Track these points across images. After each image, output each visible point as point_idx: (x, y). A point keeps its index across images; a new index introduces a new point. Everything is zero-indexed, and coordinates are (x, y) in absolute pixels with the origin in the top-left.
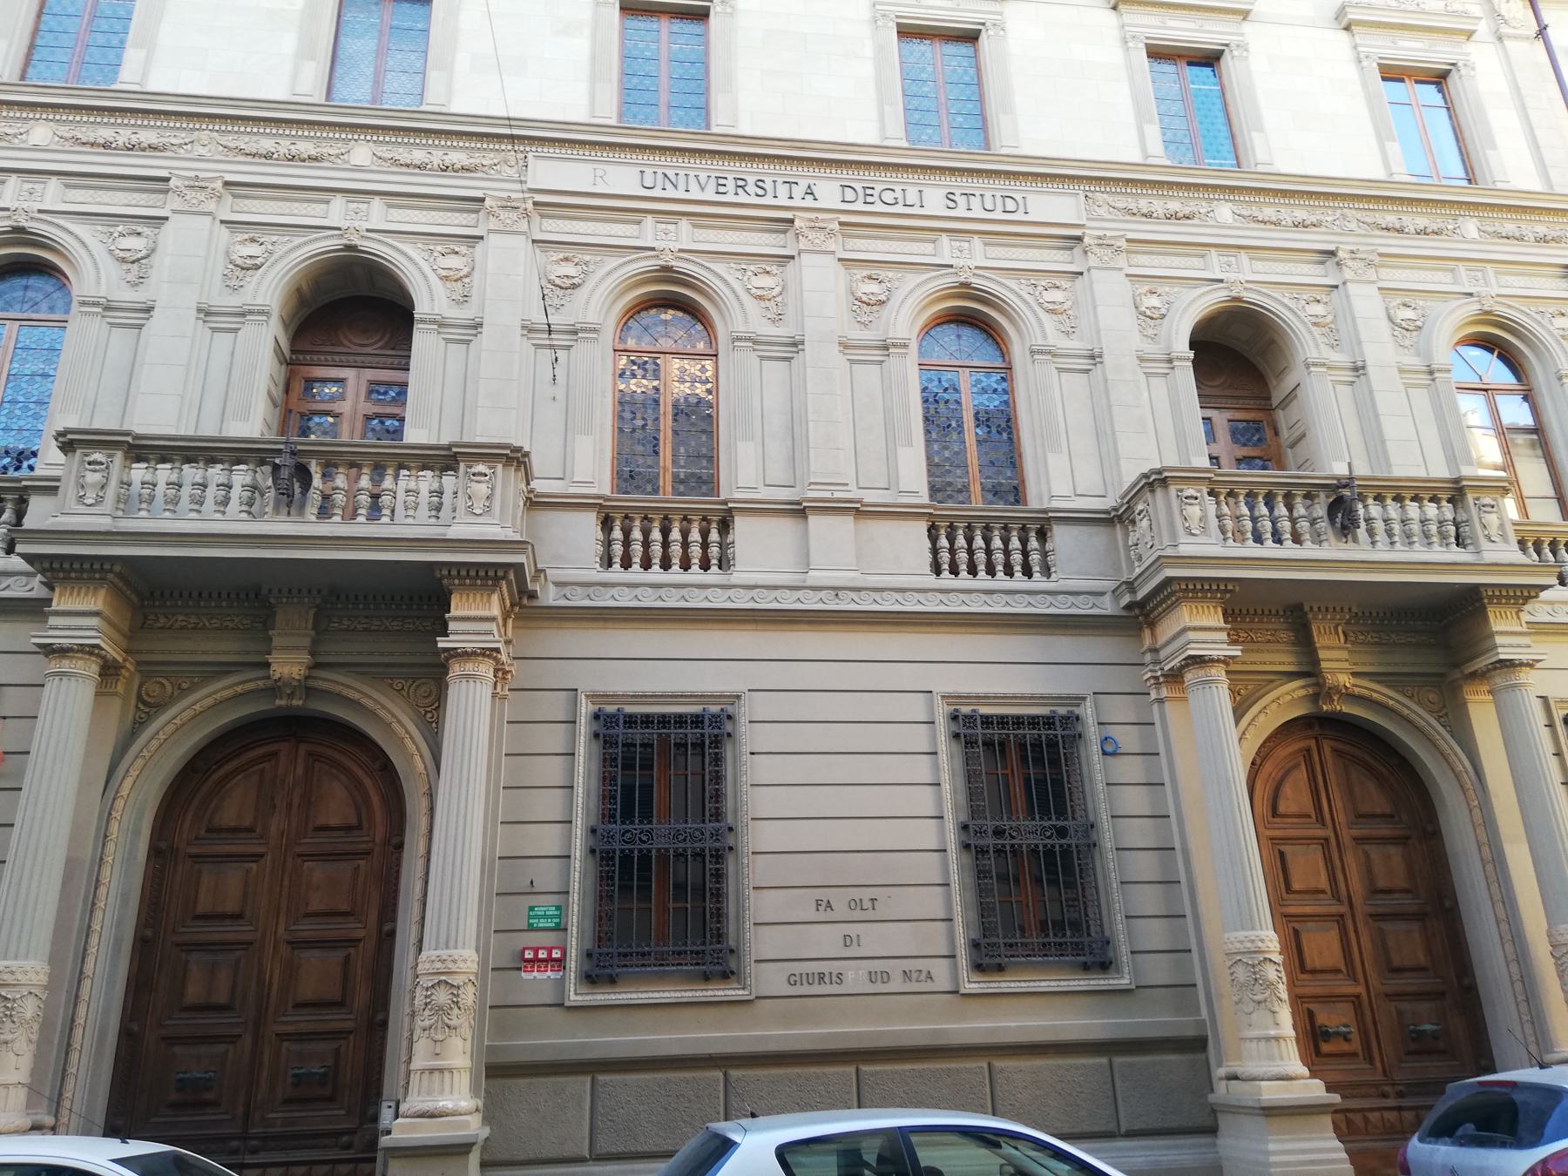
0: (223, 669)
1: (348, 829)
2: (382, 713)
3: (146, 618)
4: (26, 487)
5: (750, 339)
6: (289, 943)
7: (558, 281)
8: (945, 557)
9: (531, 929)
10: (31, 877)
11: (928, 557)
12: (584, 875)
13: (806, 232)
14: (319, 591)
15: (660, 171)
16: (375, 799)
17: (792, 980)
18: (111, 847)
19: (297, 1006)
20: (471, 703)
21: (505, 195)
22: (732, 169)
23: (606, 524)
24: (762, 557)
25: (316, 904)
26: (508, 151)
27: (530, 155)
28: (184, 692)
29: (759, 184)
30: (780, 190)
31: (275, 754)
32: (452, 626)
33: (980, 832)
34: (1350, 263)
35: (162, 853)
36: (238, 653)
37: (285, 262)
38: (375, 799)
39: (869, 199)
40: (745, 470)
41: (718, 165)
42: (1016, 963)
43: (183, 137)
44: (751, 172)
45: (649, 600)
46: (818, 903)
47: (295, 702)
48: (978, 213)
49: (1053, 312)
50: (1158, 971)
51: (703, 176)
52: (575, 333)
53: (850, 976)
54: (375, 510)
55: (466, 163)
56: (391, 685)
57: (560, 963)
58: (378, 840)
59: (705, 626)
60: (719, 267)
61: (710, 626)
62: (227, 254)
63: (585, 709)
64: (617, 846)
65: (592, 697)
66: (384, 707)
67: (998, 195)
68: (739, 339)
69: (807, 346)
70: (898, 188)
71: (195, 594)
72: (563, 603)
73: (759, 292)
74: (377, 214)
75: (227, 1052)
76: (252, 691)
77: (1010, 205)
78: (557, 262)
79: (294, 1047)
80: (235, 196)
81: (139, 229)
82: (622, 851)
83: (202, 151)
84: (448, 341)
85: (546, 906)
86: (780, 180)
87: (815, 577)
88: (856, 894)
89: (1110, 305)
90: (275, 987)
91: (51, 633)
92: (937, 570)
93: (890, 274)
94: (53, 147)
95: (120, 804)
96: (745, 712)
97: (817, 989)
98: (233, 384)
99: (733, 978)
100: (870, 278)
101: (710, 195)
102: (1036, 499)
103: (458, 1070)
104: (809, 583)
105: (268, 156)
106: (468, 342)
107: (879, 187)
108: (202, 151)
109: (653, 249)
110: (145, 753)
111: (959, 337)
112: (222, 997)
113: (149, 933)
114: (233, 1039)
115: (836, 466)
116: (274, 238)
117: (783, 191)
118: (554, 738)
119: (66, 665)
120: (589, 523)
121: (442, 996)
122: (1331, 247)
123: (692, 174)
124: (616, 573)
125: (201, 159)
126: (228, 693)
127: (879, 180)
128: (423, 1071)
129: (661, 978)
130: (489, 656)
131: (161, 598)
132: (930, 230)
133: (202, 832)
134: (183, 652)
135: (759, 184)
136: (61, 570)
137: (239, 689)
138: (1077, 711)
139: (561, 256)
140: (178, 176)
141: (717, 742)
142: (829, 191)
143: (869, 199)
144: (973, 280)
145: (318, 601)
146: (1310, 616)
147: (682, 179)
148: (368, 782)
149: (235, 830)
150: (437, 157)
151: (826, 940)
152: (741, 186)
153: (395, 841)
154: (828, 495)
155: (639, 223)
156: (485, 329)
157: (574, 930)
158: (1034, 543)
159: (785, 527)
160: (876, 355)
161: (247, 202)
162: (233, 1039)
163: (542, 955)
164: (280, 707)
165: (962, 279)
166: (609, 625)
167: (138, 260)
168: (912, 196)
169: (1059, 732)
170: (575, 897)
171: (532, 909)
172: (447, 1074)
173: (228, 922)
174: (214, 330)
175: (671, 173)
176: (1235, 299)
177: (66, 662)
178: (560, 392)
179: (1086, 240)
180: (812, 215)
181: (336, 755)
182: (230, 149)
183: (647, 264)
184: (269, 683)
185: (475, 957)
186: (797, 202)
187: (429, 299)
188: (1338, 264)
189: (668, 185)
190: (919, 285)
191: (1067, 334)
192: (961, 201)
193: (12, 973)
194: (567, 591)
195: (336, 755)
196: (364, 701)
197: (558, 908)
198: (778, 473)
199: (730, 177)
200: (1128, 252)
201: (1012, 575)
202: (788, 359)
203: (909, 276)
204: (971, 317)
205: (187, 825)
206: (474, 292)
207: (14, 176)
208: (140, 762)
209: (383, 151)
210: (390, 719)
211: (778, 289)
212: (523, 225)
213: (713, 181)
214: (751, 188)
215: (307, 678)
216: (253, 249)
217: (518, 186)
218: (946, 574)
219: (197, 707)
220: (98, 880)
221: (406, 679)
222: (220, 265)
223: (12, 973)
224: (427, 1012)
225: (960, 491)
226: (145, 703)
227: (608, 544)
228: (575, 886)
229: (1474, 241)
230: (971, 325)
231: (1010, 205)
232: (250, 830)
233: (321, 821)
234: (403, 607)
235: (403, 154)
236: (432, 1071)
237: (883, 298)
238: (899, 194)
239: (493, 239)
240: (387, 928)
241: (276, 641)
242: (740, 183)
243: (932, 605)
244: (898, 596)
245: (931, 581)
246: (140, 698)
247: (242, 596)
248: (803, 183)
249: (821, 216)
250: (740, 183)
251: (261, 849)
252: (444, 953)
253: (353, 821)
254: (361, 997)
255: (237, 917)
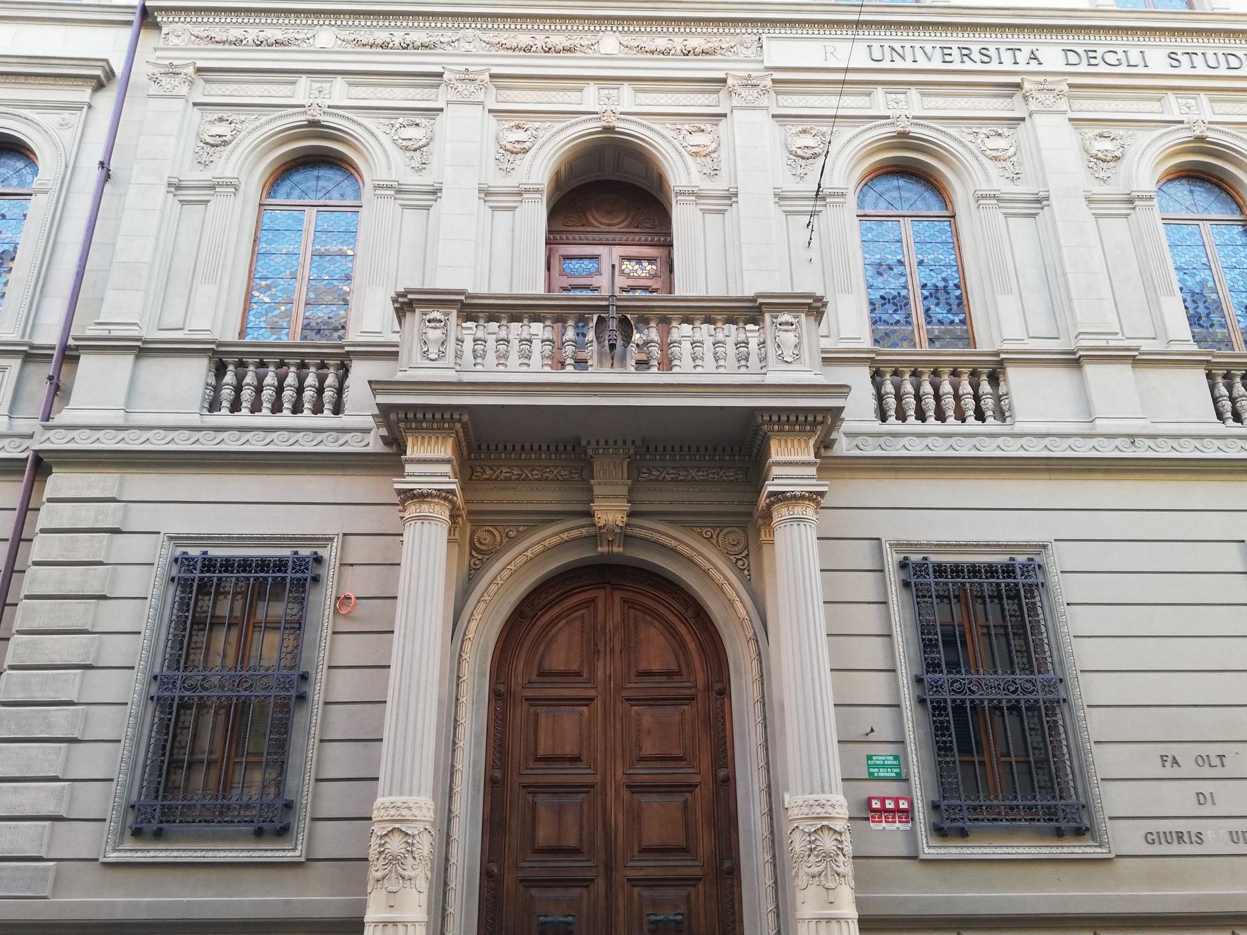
0: (549, 518)
1: (669, 674)
2: (699, 560)
3: (473, 470)
4: (348, 352)
5: (391, 187)
6: (628, 787)
7: (800, 152)
8: (891, 402)
9: (872, 778)
10: (416, 714)
11: (873, 403)
12: (917, 725)
13: (740, 90)
14: (633, 442)
15: (886, 45)
16: (692, 646)
17: (1149, 838)
18: (464, 687)
19: (644, 851)
20: (795, 546)
21: (745, 74)
22: (956, 39)
23: (220, 370)
24: (1040, 407)
25: (649, 749)
26: (748, 36)
27: (764, 37)
28: (513, 541)
29: (983, 52)
30: (1005, 56)
31: (593, 600)
32: (409, 468)
33: (936, 686)
34: (740, 90)
35: (500, 696)
36: (558, 502)
37: (551, 144)
38: (692, 646)
39: (1093, 61)
40: (1002, 322)
41: (942, 37)
42: (1021, 827)
43: (448, 36)
44: (975, 42)
45: (281, 444)
46: (1163, 759)
47: (616, 549)
48: (1202, 70)
49: (996, 158)
50: (330, 840)
51: (928, 47)
52: (520, 194)
53: (1209, 836)
54: (667, 364)
55: (706, 46)
56: (700, 534)
57: (908, 815)
58: (700, 686)
59: (1147, 476)
60: (953, 131)
61: (921, 475)
62: (497, 140)
63: (892, 559)
64: (948, 697)
65: (897, 546)
66: (700, 554)
67: (1220, 53)
68: (983, 197)
69: (1053, 199)
70: (1120, 50)
71: (518, 447)
72: (857, 453)
73: (994, 154)
74: (627, 99)
75: (581, 897)
76: (574, 539)
77: (1234, 62)
78: (510, 129)
79: (646, 893)
80: (923, 95)
81: (418, 121)
82: (954, 701)
83: (468, 47)
84: (704, 211)
85: (884, 754)
86: (1003, 48)
87: (1102, 426)
88: (1204, 749)
89: (465, 139)
90: (620, 834)
91: (408, 479)
92: (883, 417)
93: (1121, 132)
94: (621, 55)
95: (468, 645)
96: (1059, 559)
97: (1176, 849)
98: (506, 250)
99: (1088, 835)
100: (1101, 136)
101: (936, 64)
102: (986, 342)
103: (846, 920)
104: (1099, 431)
105: (528, 49)
106: (428, 208)
107: (1101, 50)
108: (468, 47)
109: (888, 117)
110: (486, 597)
111: (1191, 192)
112: (571, 841)
113: (498, 774)
114: (586, 883)
115: (1096, 317)
116: (537, 124)
117: (1007, 57)
118: (865, 586)
119: (425, 509)
120: (197, 371)
121: (396, 845)
122: (721, 75)
123: (917, 46)
124: (224, 417)
125: (468, 54)
126: (555, 540)
127: (1101, 44)
128: (377, 923)
129: (1012, 833)
130: (445, 499)
131: (500, 447)
132: (1157, 88)
133: (534, 677)
134: (662, 502)
135: (983, 52)
136: (401, 423)
137: (565, 536)
138: (320, 552)
139: (800, 128)
140: (451, 71)
141: (1031, 589)
142: (1052, 55)
143: (1093, 61)
144: (322, 118)
145: (632, 451)
146: (590, 452)
147: (908, 50)
148: (682, 629)
149: (565, 674)
150: (678, 43)
151: (1178, 798)
152: (966, 54)
153: (717, 686)
154: (1103, 343)
155: (869, 94)
156: (444, 194)
157: (915, 781)
158: (985, 387)
159: (1061, 377)
160: (1122, 209)
161: (509, 92)
162: (586, 883)
163: (890, 805)
164: (602, 554)
165: (1197, 133)
166: (900, 475)
167: (420, 148)
168: (1134, 57)
169: (1021, 580)
170: (911, 747)
171: (869, 757)
172: (844, 924)
173: (567, 765)
174: (494, 209)
175: (897, 46)
176: (608, 129)
177: (425, 507)
178: (814, 253)
179: (730, 82)
180: (1041, 79)
181: (652, 604)
182: (631, 48)
183: (1183, 135)
184: (592, 530)
185: (431, 804)
186: (1022, 67)
187: (680, 172)
188: (1025, 97)
189: (896, 57)
190: (1153, 141)
191: (1105, 181)
192: (1185, 60)
193: (409, 808)
194: (858, 441)
195: (652, 604)
196: (681, 548)
197: (896, 758)
198: (1040, 325)
199: (955, 47)
200: (1070, 97)
201: (924, 420)
202: (722, 212)
203: (1139, 133)
204: (908, 169)
205: (520, 669)
206: (723, 165)
207: (304, 77)
208: (482, 605)
209: (627, 40)
210: (706, 566)
211: (1012, 150)
212: (184, 90)
213: (938, 51)
214: (976, 56)
215: (627, 525)
216: (520, 135)
217: (760, 66)
218: (892, 419)
219: (529, 553)
220: (456, 721)
221: (714, 528)
222: (492, 149)
223: (409, 808)
224: (812, 858)
225: (938, 338)
226: (479, 551)
227: (217, 389)
228: (910, 736)
229: (609, 57)
230: (1203, 180)
231: (1234, 62)
232: (579, 674)
233: (643, 666)
234: (722, 457)
235: (365, 36)
236: (385, 924)
237: (1118, 154)
238: (1121, 55)
239: (450, 111)
240: (722, 773)
241: (597, 490)
242: (965, 52)
243: (208, 443)
244: (1197, 443)
245: (877, 426)
246: (473, 547)
247: (561, 448)
248: (1026, 50)
249: (1049, 79)
250: (965, 52)
251: (592, 693)
252: (398, 799)
253: (674, 667)
254: (705, 842)
255: (576, 759)
